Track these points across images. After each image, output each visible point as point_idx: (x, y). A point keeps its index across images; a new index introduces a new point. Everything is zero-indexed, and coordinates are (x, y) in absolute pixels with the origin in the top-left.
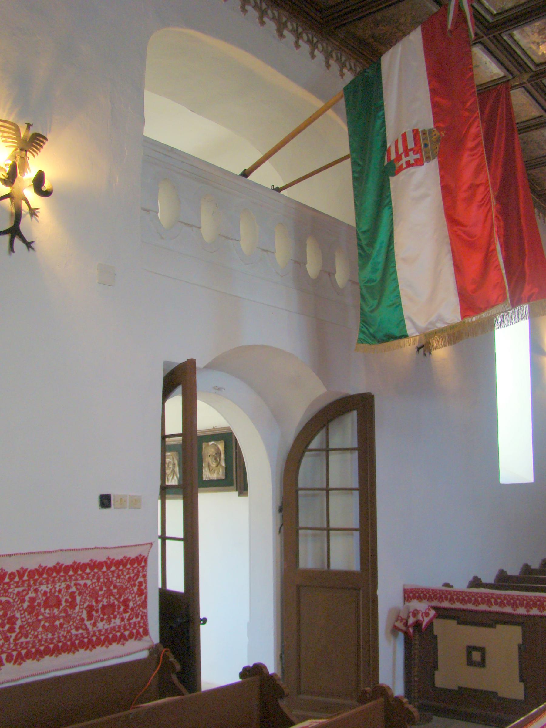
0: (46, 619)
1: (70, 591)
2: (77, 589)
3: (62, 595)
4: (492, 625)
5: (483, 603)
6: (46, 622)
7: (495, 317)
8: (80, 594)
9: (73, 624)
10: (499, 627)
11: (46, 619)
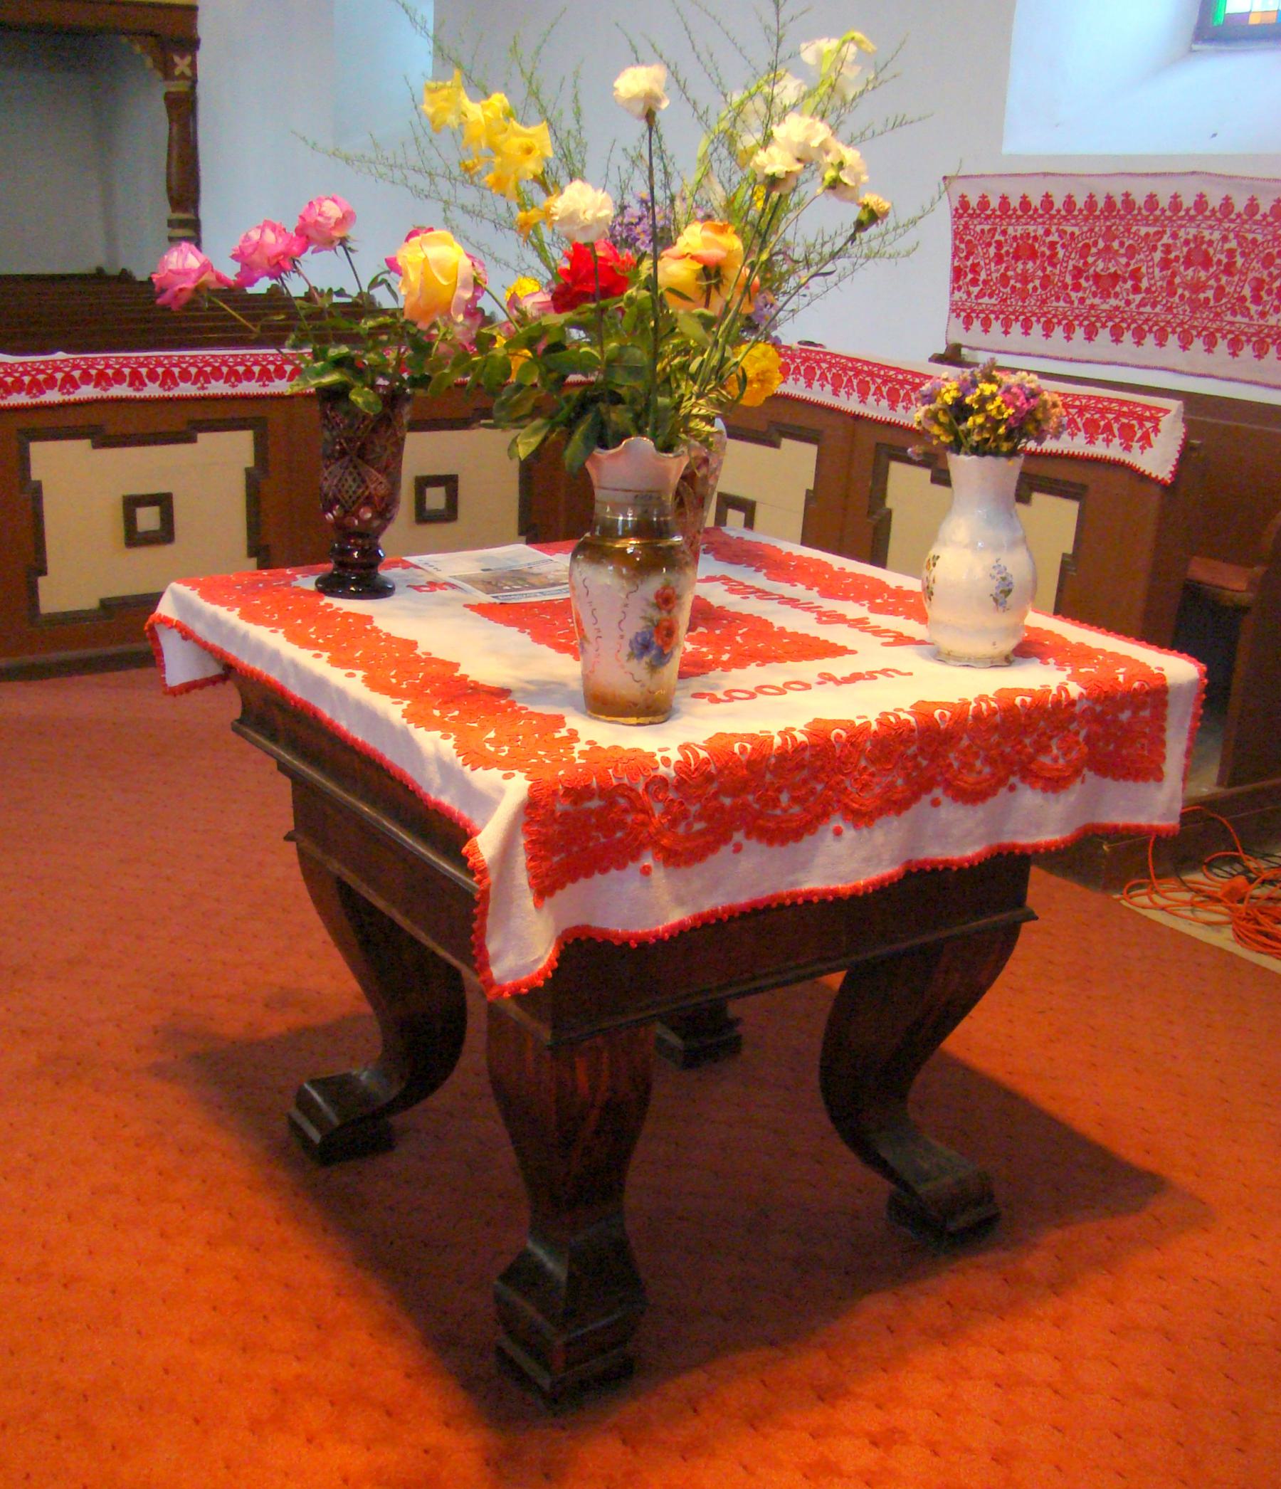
0: (1186, 286)
1: (1227, 246)
2: (1239, 244)
3: (1215, 250)
4: (185, 436)
5: (87, 383)
6: (1184, 289)
7: (552, 215)
8: (1243, 299)
9: (1226, 303)
10: (203, 437)
11: (1186, 286)
